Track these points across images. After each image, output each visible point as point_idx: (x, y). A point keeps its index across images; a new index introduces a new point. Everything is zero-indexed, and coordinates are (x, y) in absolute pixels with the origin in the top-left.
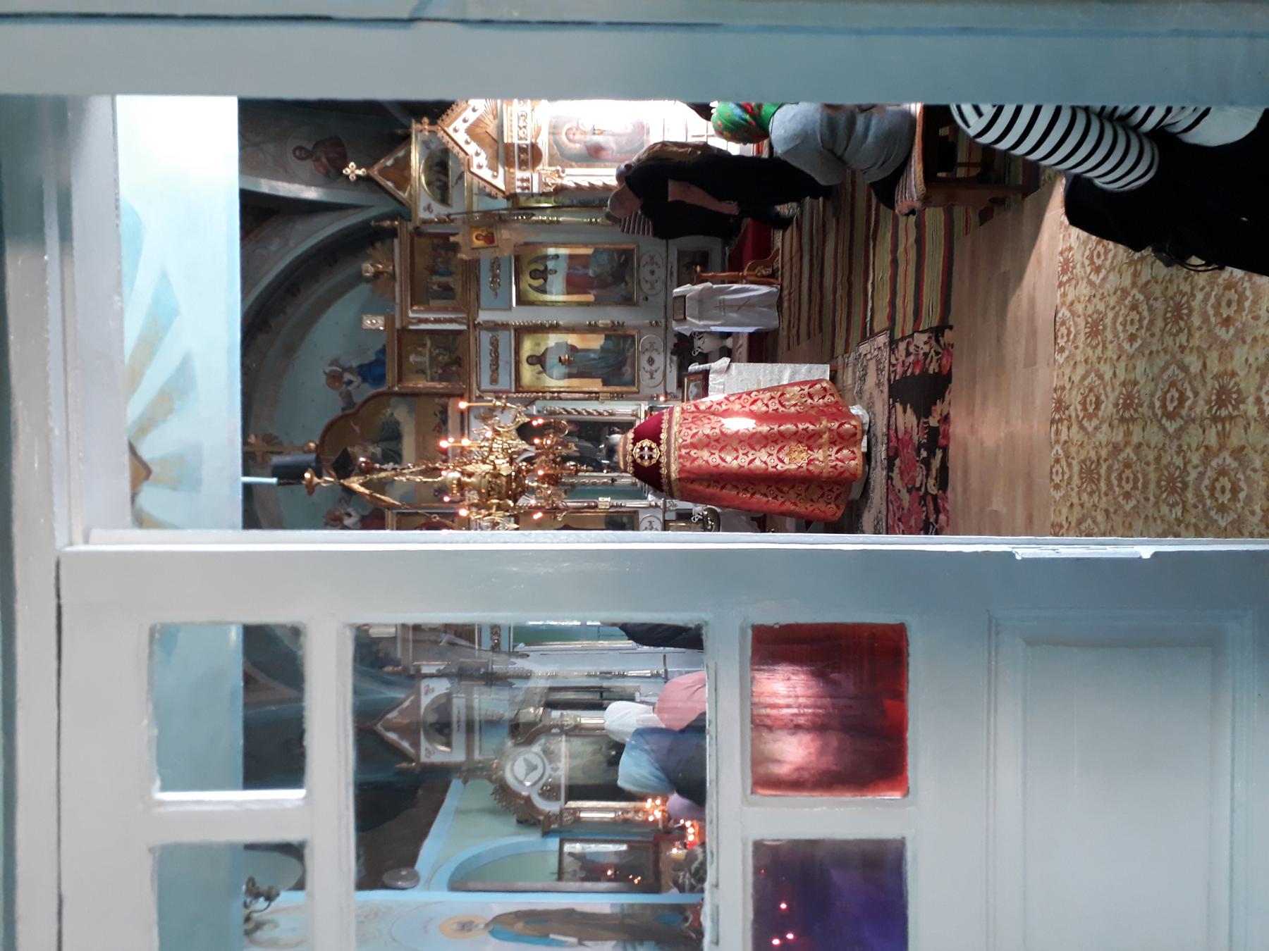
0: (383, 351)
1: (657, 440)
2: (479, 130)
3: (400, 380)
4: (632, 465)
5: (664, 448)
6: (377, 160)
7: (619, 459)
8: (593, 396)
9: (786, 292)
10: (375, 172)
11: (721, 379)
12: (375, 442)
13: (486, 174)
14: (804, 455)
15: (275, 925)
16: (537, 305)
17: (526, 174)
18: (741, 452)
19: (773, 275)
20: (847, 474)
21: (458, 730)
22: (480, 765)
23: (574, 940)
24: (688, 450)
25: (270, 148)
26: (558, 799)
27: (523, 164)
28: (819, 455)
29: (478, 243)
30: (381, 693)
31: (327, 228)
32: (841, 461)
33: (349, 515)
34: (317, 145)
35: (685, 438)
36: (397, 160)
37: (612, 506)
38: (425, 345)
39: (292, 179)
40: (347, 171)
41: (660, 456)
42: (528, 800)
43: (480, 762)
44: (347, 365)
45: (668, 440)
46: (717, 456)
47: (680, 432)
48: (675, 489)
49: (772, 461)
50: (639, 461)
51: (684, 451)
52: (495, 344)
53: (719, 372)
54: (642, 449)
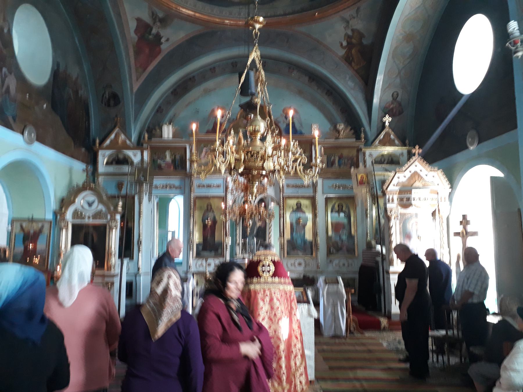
1: (275, 275)
2: (417, 177)
6: (393, 130)
8: (282, 234)
10: (387, 130)
11: (305, 312)
13: (395, 181)
16: (325, 207)
19: (351, 332)
25: (398, 80)
27: (401, 200)
29: (359, 177)
31: (360, 109)
34: (400, 104)
37: (226, 246)
39: (384, 90)
40: (387, 116)
45: (273, 283)
50: (261, 264)
53: (309, 310)
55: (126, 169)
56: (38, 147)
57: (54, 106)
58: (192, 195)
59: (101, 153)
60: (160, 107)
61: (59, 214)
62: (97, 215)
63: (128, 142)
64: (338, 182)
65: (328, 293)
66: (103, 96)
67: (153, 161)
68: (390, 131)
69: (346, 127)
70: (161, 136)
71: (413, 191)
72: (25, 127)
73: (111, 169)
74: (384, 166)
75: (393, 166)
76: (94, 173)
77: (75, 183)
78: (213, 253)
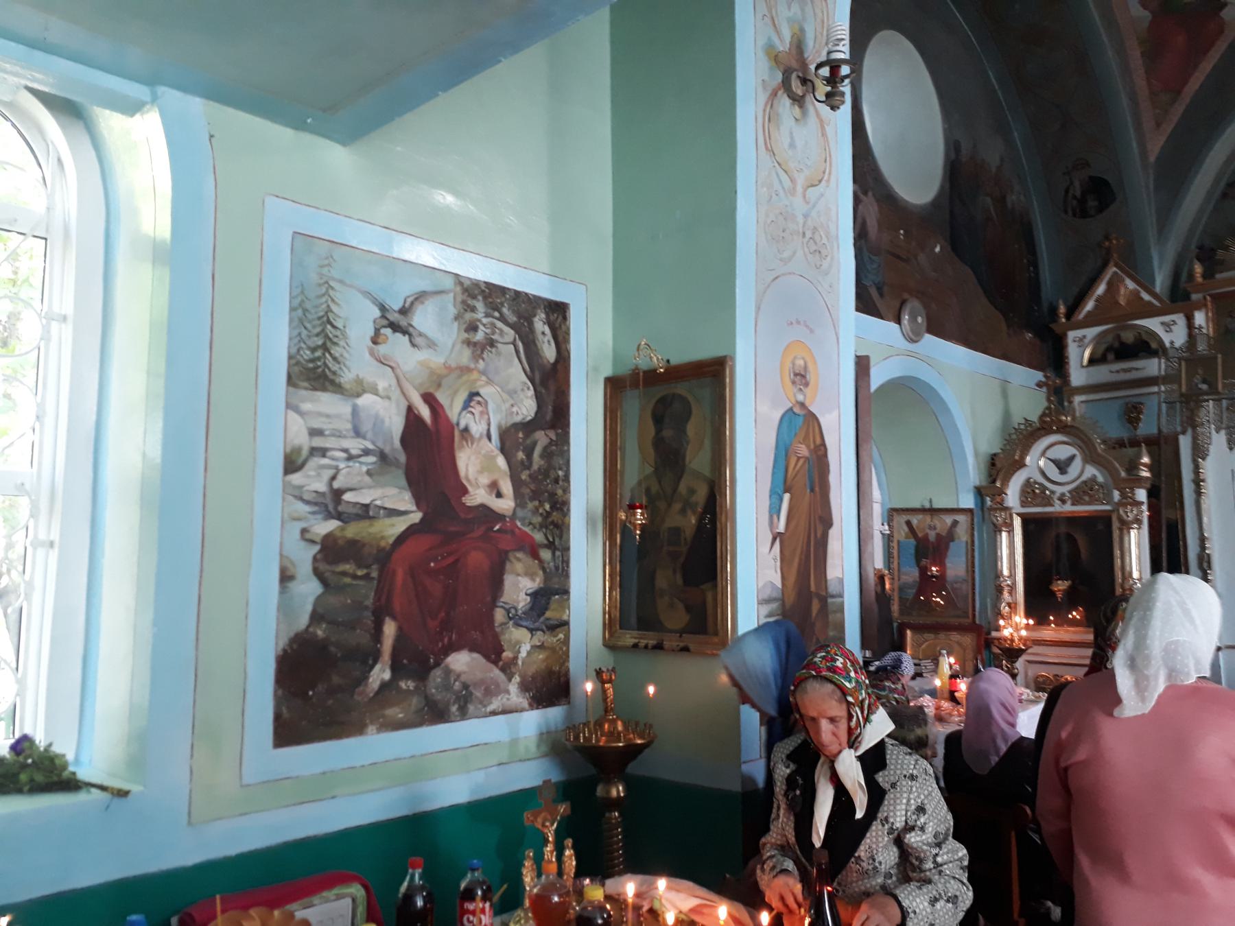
15: (801, 120)
21: (1111, 372)
22: (1066, 404)
23: (781, 527)
26: (1024, 504)
30: (1160, 268)
42: (1021, 465)
43: (1070, 402)
55: (1153, 367)
56: (932, 344)
57: (955, 245)
59: (1072, 335)
61: (990, 491)
62: (1083, 492)
63: (1146, 297)
66: (1067, 191)
72: (903, 303)
73: (1103, 373)
77: (1017, 419)
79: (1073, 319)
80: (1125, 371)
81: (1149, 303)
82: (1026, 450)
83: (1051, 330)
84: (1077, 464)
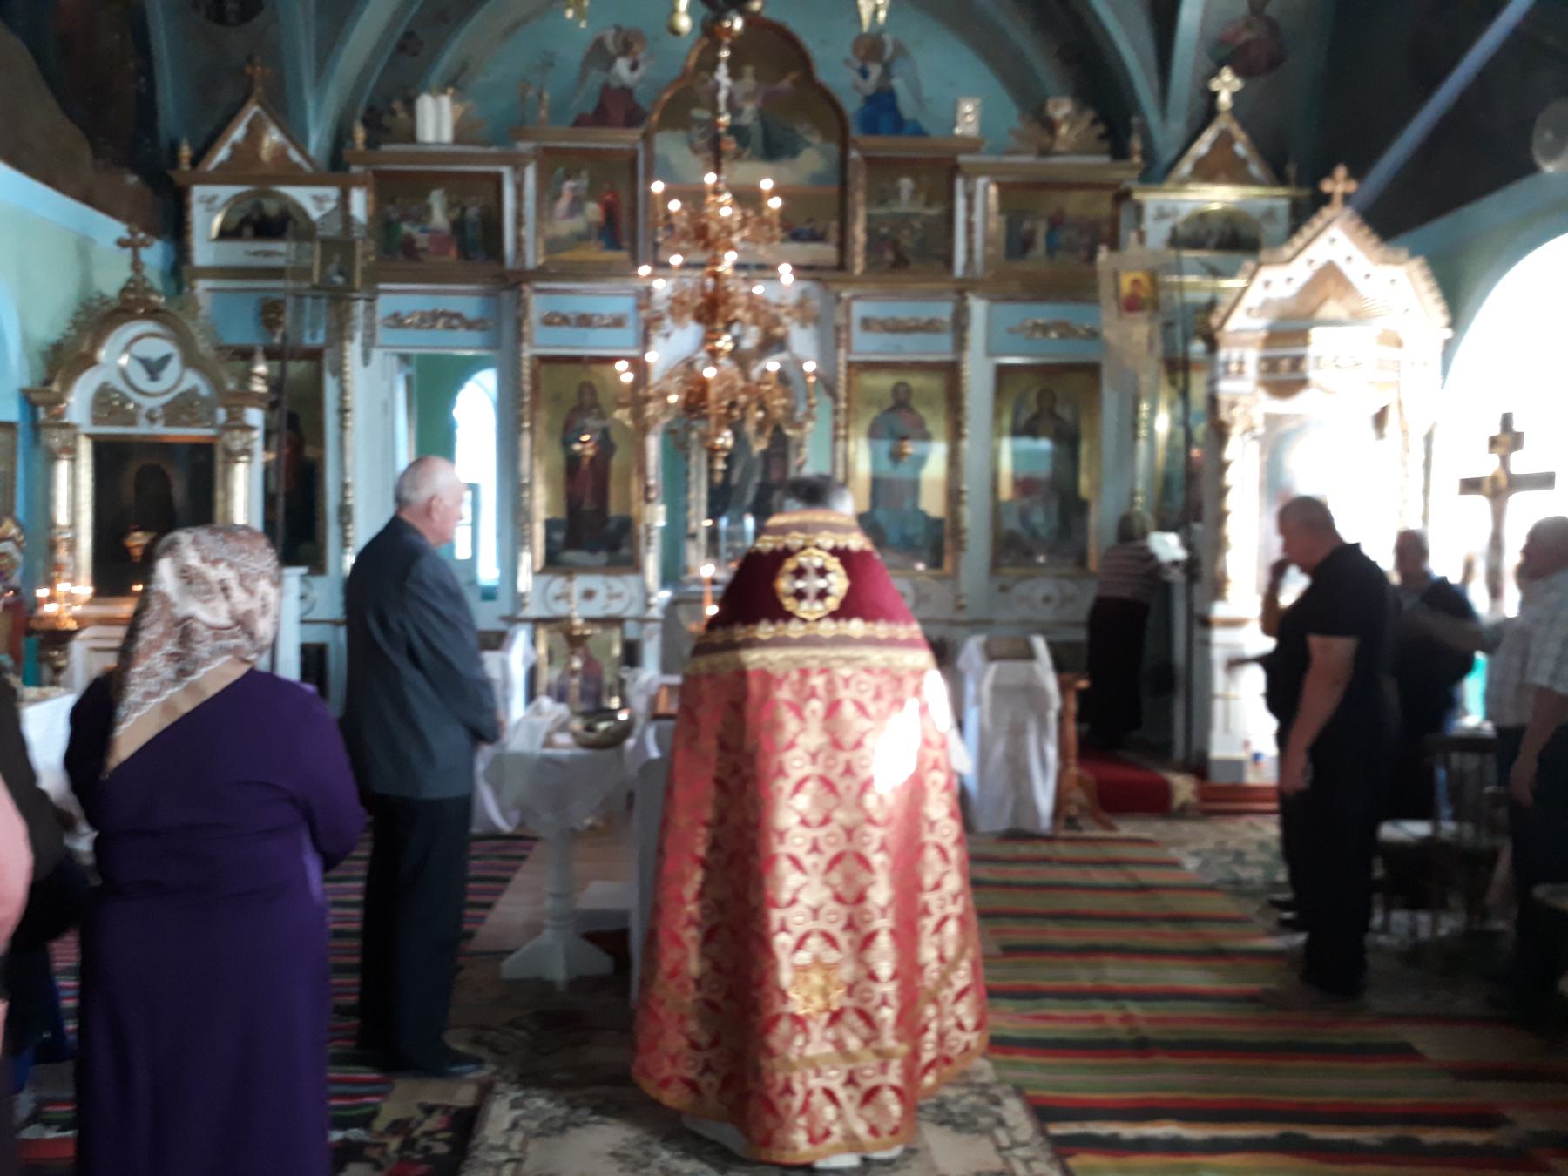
0: (919, 132)
1: (846, 610)
2: (1331, 284)
3: (871, 161)
4: (780, 546)
5: (828, 628)
6: (1245, 126)
7: (793, 512)
9: (1043, 849)
10: (1223, 123)
12: (762, 115)
13: (1254, 296)
14: (818, 1001)
17: (1251, 369)
18: (821, 833)
20: (770, 1122)
24: (821, 691)
26: (97, 421)
27: (1270, 365)
28: (818, 1044)
32: (805, 1108)
33: (634, 67)
34: (1273, 26)
35: (853, 683)
36: (1243, 162)
38: (928, 204)
40: (1227, 75)
41: (804, 621)
42: (89, 361)
43: (192, 288)
44: (896, 70)
45: (843, 641)
46: (808, 769)
47: (868, 670)
48: (717, 659)
49: (798, 919)
50: (790, 565)
51: (818, 681)
52: (930, 327)
54: (822, 572)
58: (527, 352)
59: (198, 192)
60: (409, 35)
62: (181, 408)
63: (295, 156)
64: (1044, 312)
65: (997, 689)
67: (383, 224)
68: (1235, 129)
69: (1079, 110)
70: (411, 136)
71: (1316, 334)
73: (239, 253)
74: (1204, 255)
75: (1233, 257)
76: (180, 268)
78: (602, 557)
79: (200, 168)
80: (267, 254)
81: (296, 166)
82: (98, 339)
83: (170, 181)
84: (174, 367)
